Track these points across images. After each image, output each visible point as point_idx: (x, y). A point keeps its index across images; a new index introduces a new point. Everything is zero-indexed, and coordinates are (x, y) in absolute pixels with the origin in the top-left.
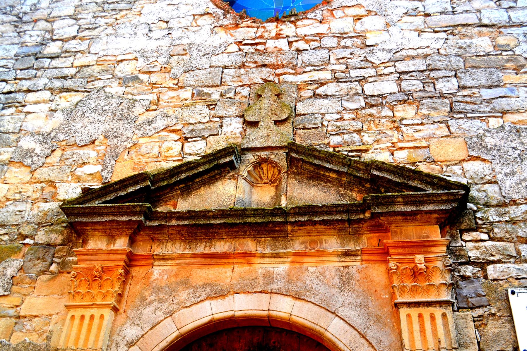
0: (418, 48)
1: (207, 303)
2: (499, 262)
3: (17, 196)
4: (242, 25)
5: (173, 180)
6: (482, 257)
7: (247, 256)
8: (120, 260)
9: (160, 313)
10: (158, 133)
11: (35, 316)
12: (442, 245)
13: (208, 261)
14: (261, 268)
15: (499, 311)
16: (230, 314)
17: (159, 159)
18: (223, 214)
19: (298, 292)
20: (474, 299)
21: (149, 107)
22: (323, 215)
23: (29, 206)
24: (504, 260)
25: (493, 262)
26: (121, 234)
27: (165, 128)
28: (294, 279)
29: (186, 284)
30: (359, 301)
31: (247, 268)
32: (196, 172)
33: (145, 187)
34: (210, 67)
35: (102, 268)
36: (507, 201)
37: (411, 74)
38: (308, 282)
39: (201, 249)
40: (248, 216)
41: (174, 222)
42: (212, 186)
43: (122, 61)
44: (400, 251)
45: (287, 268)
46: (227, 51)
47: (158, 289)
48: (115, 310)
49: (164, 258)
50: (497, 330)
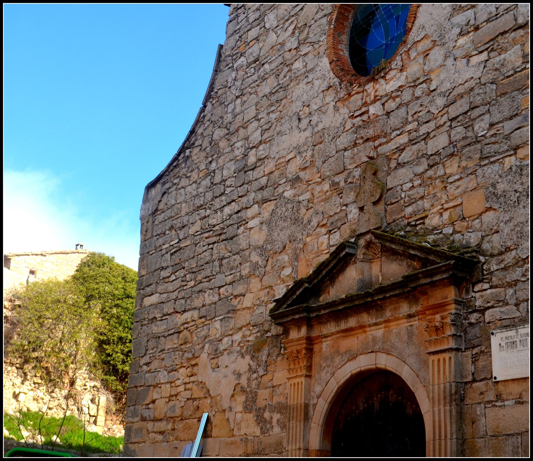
0: (465, 82)
1: (348, 364)
2: (492, 307)
3: (258, 302)
4: (353, 93)
5: (320, 277)
6: (483, 305)
7: (362, 327)
8: (303, 344)
9: (328, 374)
10: (315, 230)
11: (280, 385)
12: (451, 304)
13: (345, 334)
14: (371, 334)
15: (486, 349)
16: (359, 370)
17: (318, 254)
18: (343, 301)
19: (388, 349)
20: (475, 341)
21: (308, 206)
22: (390, 292)
23: (264, 308)
24: (495, 305)
25: (489, 308)
26: (302, 324)
27: (318, 225)
28: (386, 340)
29: (338, 352)
30: (416, 351)
31: (364, 335)
32: (330, 267)
33: (304, 289)
34: (337, 152)
35: (297, 351)
36: (503, 250)
37: (458, 120)
38: (393, 341)
39: (343, 326)
40: (355, 300)
41: (323, 312)
42: (345, 273)
43: (289, 161)
44: (431, 312)
45: (98, 429)
46: (346, 130)
47: (326, 359)
48: (309, 376)
49: (326, 336)
50: (484, 363)
